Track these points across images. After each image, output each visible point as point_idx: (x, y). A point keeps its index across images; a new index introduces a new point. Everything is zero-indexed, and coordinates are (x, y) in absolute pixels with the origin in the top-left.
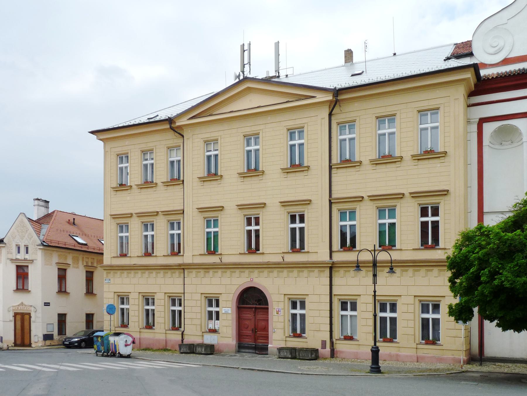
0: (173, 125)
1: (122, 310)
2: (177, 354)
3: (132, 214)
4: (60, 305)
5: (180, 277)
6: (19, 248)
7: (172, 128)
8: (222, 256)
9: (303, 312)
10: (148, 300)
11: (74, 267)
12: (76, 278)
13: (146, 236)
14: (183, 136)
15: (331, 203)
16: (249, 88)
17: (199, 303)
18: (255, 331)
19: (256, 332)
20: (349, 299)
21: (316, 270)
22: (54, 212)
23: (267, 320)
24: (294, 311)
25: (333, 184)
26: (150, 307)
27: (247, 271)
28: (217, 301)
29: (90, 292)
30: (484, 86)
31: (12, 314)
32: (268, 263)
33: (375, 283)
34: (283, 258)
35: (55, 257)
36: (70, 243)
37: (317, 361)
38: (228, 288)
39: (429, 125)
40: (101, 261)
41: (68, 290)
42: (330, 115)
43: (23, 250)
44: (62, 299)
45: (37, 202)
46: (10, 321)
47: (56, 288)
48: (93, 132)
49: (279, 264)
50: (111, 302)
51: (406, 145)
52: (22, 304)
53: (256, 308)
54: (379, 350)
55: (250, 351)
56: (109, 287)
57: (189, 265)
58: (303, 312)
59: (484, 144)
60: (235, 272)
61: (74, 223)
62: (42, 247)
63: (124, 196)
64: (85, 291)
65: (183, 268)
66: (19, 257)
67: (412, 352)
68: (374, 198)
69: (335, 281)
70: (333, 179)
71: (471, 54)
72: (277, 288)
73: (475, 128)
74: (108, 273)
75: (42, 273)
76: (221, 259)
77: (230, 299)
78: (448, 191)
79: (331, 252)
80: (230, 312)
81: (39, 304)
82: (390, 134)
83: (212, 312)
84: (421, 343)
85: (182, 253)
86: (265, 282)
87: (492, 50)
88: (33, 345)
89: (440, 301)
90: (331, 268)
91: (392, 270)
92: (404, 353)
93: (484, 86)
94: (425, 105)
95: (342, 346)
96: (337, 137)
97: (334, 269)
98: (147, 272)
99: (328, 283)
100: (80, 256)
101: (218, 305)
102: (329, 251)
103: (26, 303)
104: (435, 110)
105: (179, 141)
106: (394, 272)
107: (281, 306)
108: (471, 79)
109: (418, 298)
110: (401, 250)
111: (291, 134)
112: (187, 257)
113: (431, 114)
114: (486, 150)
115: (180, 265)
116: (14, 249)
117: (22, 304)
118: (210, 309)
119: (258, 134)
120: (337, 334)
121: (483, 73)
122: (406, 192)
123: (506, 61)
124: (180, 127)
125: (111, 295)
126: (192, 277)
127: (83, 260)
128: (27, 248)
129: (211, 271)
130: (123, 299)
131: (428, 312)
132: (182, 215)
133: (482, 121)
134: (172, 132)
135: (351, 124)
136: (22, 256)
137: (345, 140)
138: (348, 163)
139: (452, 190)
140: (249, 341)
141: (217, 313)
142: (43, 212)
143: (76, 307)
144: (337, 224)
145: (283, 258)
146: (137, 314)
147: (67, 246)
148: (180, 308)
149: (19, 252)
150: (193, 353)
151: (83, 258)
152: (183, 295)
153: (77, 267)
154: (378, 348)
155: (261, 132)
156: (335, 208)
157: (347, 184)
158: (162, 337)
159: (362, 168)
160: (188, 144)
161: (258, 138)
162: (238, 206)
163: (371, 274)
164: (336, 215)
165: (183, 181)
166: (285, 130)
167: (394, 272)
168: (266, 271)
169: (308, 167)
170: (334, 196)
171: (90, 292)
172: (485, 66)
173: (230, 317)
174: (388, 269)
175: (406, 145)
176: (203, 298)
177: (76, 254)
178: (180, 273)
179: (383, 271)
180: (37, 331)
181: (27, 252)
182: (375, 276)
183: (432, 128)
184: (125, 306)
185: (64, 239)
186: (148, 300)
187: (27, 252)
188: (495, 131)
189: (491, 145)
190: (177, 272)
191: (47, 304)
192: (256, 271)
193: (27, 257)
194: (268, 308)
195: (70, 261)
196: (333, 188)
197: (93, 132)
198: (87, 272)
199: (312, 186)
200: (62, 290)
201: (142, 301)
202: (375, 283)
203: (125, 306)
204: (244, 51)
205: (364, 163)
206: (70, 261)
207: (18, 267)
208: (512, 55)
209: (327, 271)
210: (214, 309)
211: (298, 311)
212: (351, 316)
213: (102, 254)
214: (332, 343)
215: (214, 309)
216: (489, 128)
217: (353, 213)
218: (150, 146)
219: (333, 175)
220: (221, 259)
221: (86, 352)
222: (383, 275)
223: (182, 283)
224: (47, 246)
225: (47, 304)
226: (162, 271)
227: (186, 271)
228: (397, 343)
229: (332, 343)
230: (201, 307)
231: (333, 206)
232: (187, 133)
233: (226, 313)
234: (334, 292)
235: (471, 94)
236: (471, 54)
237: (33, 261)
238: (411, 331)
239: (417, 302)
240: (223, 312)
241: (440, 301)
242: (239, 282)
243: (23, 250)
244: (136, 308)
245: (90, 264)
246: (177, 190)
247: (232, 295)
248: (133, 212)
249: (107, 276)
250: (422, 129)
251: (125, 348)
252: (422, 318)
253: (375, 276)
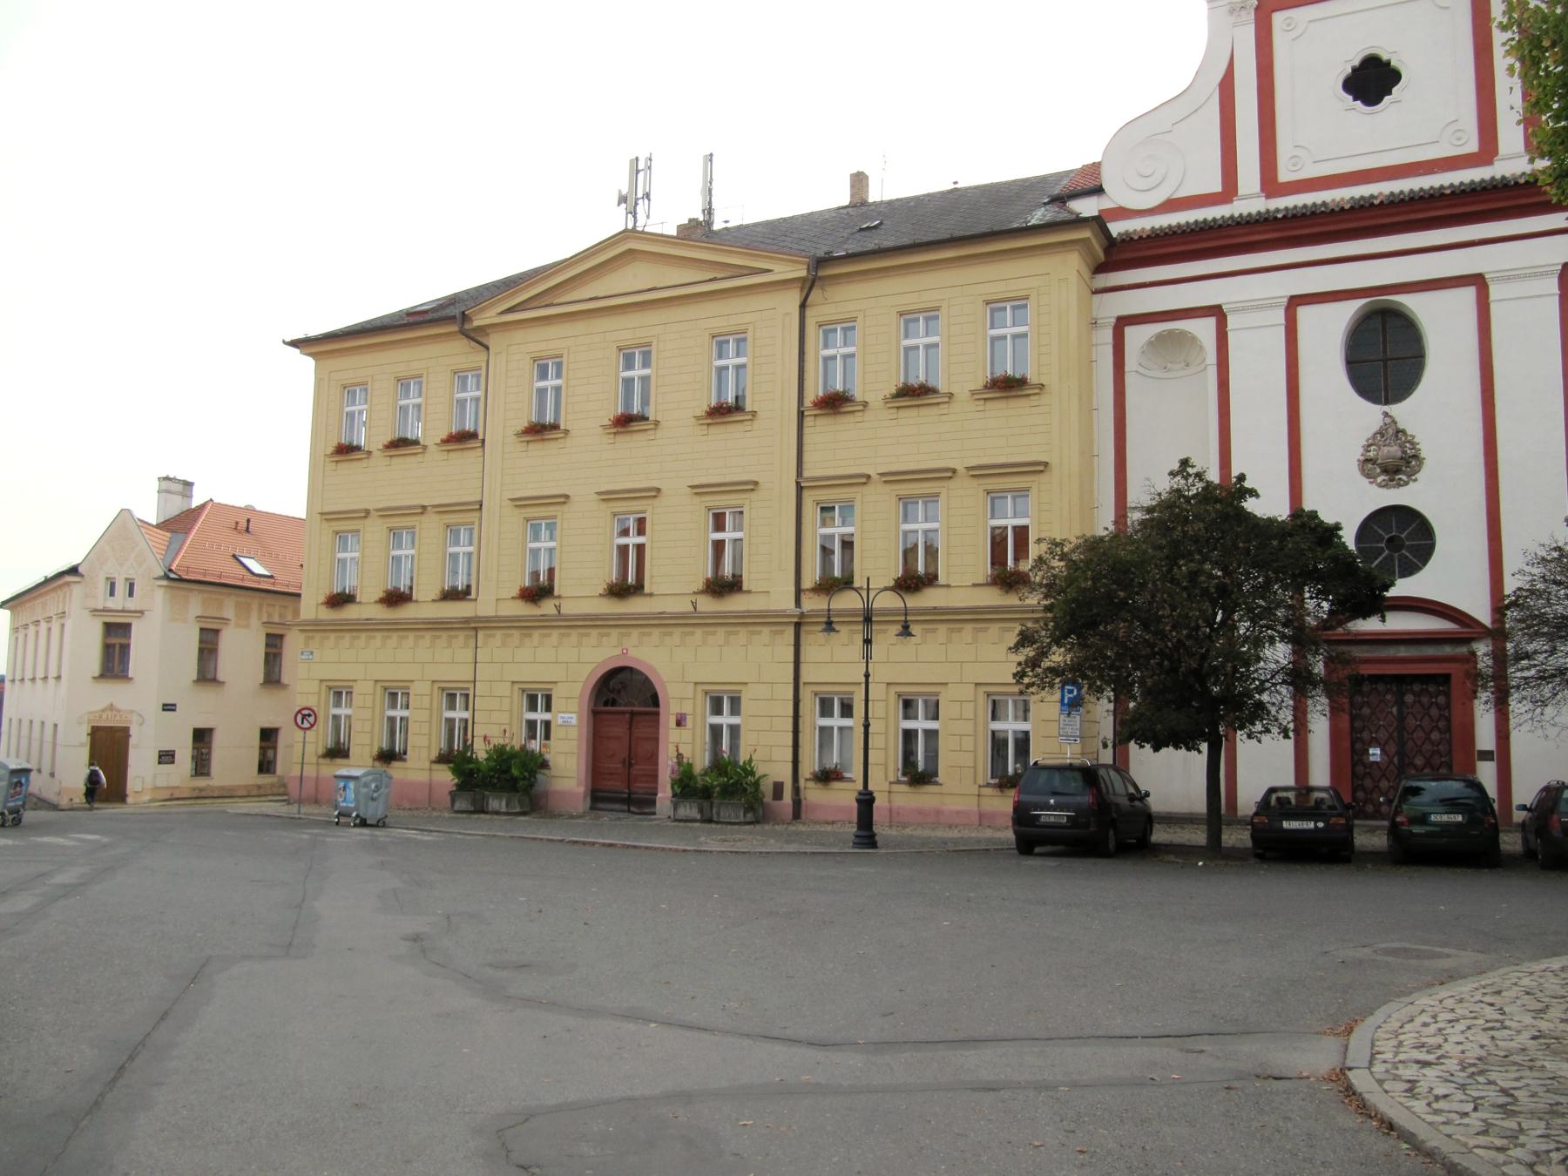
0: (467, 326)
1: (336, 718)
2: (1253, 861)
3: (367, 512)
4: (199, 709)
5: (466, 646)
6: (113, 585)
7: (465, 333)
8: (563, 602)
9: (735, 720)
10: (394, 695)
11: (237, 626)
12: (241, 650)
13: (719, 546)
14: (487, 348)
15: (800, 489)
16: (631, 252)
17: (506, 703)
18: (629, 763)
19: (630, 765)
20: (837, 693)
21: (766, 630)
22: (203, 506)
23: (656, 740)
24: (716, 720)
25: (805, 448)
26: (398, 713)
27: (615, 632)
28: (548, 699)
29: (272, 677)
30: (1119, 253)
31: (85, 730)
32: (661, 616)
33: (867, 657)
34: (694, 604)
35: (196, 605)
36: (232, 574)
37: (758, 827)
38: (571, 667)
39: (1009, 331)
40: (297, 612)
41: (221, 676)
42: (803, 306)
43: (121, 588)
44: (208, 695)
45: (165, 484)
46: (82, 745)
47: (192, 670)
48: (295, 344)
49: (683, 616)
50: (311, 702)
51: (961, 373)
52: (111, 707)
53: (632, 714)
54: (872, 800)
55: (617, 806)
56: (309, 667)
57: (487, 619)
58: (735, 720)
59: (1127, 369)
60: (588, 635)
61: (247, 530)
62: (165, 583)
63: (350, 470)
64: (261, 679)
65: (474, 626)
66: (112, 603)
67: (970, 804)
68: (892, 478)
69: (808, 653)
70: (807, 439)
71: (1098, 190)
72: (679, 669)
73: (1107, 336)
74: (308, 639)
75: (163, 643)
76: (558, 608)
77: (577, 693)
78: (1046, 464)
79: (799, 592)
80: (574, 721)
81: (152, 709)
82: (928, 347)
83: (535, 722)
84: (899, 782)
85: (473, 596)
86: (658, 657)
87: (1144, 184)
88: (130, 800)
89: (937, 694)
90: (798, 625)
91: (906, 631)
92: (952, 804)
93: (1119, 253)
94: (997, 290)
95: (813, 794)
96: (817, 353)
97: (804, 629)
98: (395, 636)
99: (791, 658)
100: (255, 602)
101: (548, 708)
102: (793, 589)
103: (121, 704)
104: (1020, 303)
105: (479, 358)
106: (910, 634)
107: (687, 708)
108: (1094, 241)
109: (983, 689)
110: (948, 586)
111: (721, 345)
112: (485, 604)
113: (1014, 308)
114: (1130, 379)
115: (467, 620)
116: (102, 588)
117: (111, 707)
118: (532, 716)
119: (649, 344)
120: (809, 765)
121: (1116, 228)
122: (959, 465)
123: (1171, 205)
124: (482, 330)
125: (314, 686)
126: (493, 647)
127: (260, 610)
128: (132, 586)
129: (536, 634)
130: (339, 694)
131: (831, 715)
132: (477, 514)
133: (1123, 322)
134: (465, 341)
135: (849, 326)
136: (119, 601)
137: (834, 358)
138: (834, 403)
139: (1054, 462)
140: (616, 784)
141: (547, 724)
142: (176, 506)
143: (237, 713)
144: (815, 532)
145: (694, 604)
146: (368, 728)
147: (223, 581)
148: (465, 715)
149: (112, 594)
150: (483, 812)
151: (261, 606)
152: (471, 686)
153: (247, 626)
154: (871, 793)
155: (751, 328)
156: (809, 499)
157: (836, 447)
158: (423, 777)
159: (868, 415)
160: (498, 363)
161: (744, 340)
162: (599, 493)
163: (859, 639)
164: (811, 513)
165: (483, 441)
166: (707, 338)
167: (910, 634)
168: (656, 632)
169: (754, 413)
170: (806, 474)
171: (272, 677)
172: (1122, 213)
173: (574, 733)
174: (898, 628)
175: (961, 373)
176: (700, 696)
177: (244, 597)
178: (467, 637)
179: (885, 632)
180: (142, 771)
181: (131, 594)
182: (868, 642)
183: (1015, 337)
184: (342, 711)
185: (219, 567)
186: (394, 695)
187: (131, 594)
188: (1150, 343)
189: (1142, 370)
190: (461, 635)
191: (169, 707)
192: (635, 632)
193: (131, 604)
194: (657, 714)
195: (229, 612)
196: (806, 457)
197: (295, 344)
198: (268, 635)
199: (761, 451)
200: (207, 675)
201: (381, 698)
202: (867, 657)
203: (342, 711)
204: (638, 172)
205: (871, 405)
206: (229, 612)
207: (109, 628)
208: (1181, 194)
209: (790, 632)
210: (540, 716)
211: (725, 720)
212: (841, 729)
213: (299, 595)
214: (796, 790)
215: (540, 716)
216: (1137, 336)
217: (848, 508)
218: (928, 299)
219: (806, 431)
220: (558, 608)
221: (740, 847)
222: (886, 640)
223: (471, 659)
224: (175, 580)
225: (169, 707)
226: (428, 635)
227: (481, 634)
228: (936, 783)
229: (796, 790)
230: (431, 709)
231: (806, 494)
232: (494, 341)
233: (566, 725)
234: (804, 678)
235: (1100, 269)
236: (1098, 190)
237: (142, 612)
238: (967, 759)
239: (981, 698)
240: (560, 721)
241: (937, 694)
242: (593, 656)
243: (121, 588)
244: (424, 715)
245: (276, 619)
246: (465, 460)
247: (579, 686)
248: (370, 507)
249: (307, 645)
250: (994, 339)
251: (372, 804)
252: (993, 732)
253: (868, 642)
